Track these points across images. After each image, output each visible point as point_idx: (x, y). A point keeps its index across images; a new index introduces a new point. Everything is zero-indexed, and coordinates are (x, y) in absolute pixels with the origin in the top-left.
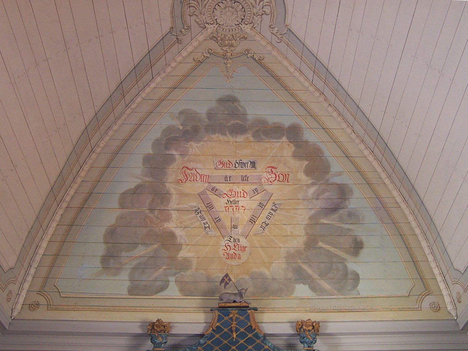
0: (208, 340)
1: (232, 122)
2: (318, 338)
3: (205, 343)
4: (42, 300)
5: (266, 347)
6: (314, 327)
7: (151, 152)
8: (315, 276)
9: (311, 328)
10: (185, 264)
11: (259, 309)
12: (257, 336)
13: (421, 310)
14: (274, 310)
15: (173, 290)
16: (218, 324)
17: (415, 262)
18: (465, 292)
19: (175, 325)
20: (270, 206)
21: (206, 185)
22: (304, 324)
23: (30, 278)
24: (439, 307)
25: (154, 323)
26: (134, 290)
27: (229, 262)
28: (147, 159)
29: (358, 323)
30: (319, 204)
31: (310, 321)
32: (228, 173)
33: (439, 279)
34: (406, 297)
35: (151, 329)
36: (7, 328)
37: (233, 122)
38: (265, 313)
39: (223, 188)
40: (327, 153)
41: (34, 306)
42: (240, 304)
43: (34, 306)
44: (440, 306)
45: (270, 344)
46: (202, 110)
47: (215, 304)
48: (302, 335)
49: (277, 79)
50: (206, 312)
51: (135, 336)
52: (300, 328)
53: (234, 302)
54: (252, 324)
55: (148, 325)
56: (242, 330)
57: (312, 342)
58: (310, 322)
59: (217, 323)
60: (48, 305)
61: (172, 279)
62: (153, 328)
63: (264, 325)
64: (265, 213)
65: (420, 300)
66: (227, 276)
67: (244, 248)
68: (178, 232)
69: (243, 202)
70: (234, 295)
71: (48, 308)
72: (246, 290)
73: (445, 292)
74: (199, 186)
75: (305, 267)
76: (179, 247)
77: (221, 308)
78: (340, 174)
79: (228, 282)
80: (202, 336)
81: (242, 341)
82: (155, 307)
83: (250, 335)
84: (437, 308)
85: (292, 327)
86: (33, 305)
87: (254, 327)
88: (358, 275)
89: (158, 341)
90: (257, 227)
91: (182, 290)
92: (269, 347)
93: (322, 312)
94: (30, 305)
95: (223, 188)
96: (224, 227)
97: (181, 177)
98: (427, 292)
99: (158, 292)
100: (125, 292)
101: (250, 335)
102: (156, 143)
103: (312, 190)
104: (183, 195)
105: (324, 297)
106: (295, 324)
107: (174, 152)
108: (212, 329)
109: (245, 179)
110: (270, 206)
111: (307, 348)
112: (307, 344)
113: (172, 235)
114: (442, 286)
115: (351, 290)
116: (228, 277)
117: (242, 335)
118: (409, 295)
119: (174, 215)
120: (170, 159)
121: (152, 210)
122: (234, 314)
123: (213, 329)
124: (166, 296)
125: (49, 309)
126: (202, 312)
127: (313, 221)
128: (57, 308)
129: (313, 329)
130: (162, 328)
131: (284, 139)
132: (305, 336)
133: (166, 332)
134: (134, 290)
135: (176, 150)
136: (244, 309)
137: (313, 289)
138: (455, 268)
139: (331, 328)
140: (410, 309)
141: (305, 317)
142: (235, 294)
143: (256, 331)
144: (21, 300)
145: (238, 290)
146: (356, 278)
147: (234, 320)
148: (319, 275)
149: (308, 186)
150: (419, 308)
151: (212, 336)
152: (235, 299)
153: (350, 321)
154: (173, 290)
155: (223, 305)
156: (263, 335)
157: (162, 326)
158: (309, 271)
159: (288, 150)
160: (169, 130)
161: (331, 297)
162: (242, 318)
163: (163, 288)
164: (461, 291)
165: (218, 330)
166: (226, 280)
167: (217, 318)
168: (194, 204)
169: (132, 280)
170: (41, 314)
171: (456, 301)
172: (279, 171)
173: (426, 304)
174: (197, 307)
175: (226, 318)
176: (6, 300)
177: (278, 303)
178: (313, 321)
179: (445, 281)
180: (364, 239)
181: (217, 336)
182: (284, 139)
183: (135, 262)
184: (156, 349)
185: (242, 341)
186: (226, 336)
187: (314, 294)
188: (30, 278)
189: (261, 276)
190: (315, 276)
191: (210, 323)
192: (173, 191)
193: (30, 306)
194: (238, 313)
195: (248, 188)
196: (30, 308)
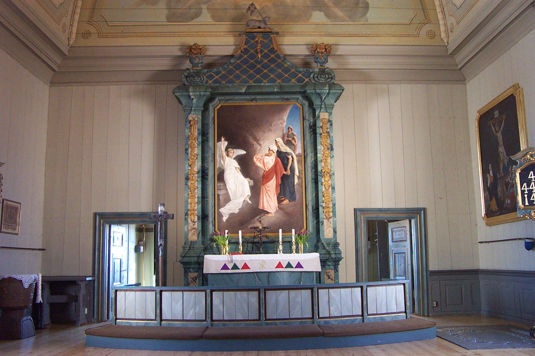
0: (237, 60)
2: (329, 58)
3: (235, 62)
4: (92, 29)
5: (286, 66)
6: (326, 49)
9: (323, 50)
11: (280, 33)
12: (278, 56)
13: (418, 37)
14: (292, 34)
15: (206, 17)
16: (245, 47)
18: (458, 25)
19: (209, 47)
22: (318, 47)
23: (78, 10)
24: (435, 35)
25: (191, 47)
26: (171, 18)
31: (323, 45)
33: (438, 10)
34: (407, 25)
35: (189, 52)
36: (67, 54)
38: (285, 36)
41: (86, 35)
42: (264, 29)
43: (86, 35)
44: (436, 34)
45: (289, 63)
48: (316, 56)
50: (235, 36)
51: (176, 57)
52: (315, 50)
53: (259, 28)
54: (274, 46)
55: (186, 48)
56: (266, 51)
57: (324, 62)
58: (323, 46)
59: (245, 45)
60: (98, 33)
61: (204, 7)
62: (191, 51)
63: (284, 47)
65: (419, 28)
66: (252, 5)
70: (259, 22)
71: (99, 36)
72: (269, 18)
73: (441, 22)
77: (248, 33)
79: (254, 10)
80: (232, 56)
81: (266, 61)
82: (191, 32)
83: (272, 56)
84: (432, 35)
85: (308, 49)
86: (85, 34)
87: (276, 49)
88: (368, 4)
89: (195, 62)
91: (213, 17)
92: (288, 65)
93: (334, 36)
94: (82, 33)
98: (427, 20)
100: (164, 19)
101: (272, 56)
105: (337, 23)
106: (311, 46)
108: (240, 51)
111: (320, 67)
112: (320, 64)
114: (440, 16)
115: (360, 17)
116: (254, 6)
117: (265, 56)
118: (410, 24)
122: (259, 38)
123: (241, 51)
124: (199, 22)
125: (100, 37)
126: (231, 36)
129: (325, 51)
130: (198, 51)
132: (318, 57)
133: (202, 54)
134: (171, 18)
136: (267, 34)
137: (328, 16)
138: (453, 3)
139: (341, 51)
140: (408, 36)
141: (320, 40)
142: (260, 21)
143: (277, 52)
144: (75, 30)
145: (263, 18)
147: (259, 43)
148: (334, 4)
150: (417, 34)
151: (241, 57)
152: (259, 26)
153: (358, 45)
154: (206, 17)
155: (250, 30)
156: (283, 56)
157: (198, 49)
161: (343, 23)
162: (266, 41)
163: (197, 15)
164: (455, 23)
165: (246, 51)
166: (252, 8)
167: (244, 41)
169: (169, 8)
170: (94, 41)
171: (449, 30)
173: (423, 31)
174: (227, 32)
175: (252, 41)
176: (62, 32)
177: (297, 28)
178: (326, 43)
179: (443, 12)
181: (245, 56)
184: (194, 68)
185: (266, 61)
186: (252, 57)
187: (329, 20)
188: (78, 10)
191: (239, 45)
193: (83, 35)
194: (262, 37)
196: (83, 36)
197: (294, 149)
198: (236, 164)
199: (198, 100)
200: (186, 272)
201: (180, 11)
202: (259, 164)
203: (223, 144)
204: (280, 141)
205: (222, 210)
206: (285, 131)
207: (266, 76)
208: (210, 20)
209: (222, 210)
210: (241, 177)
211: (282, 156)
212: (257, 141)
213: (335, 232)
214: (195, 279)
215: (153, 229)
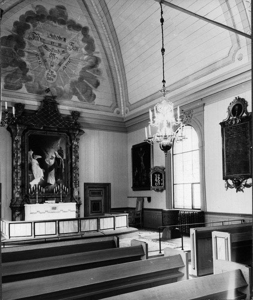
1: (60, 18)
7: (18, 20)
8: (80, 93)
10: (30, 79)
15: (24, 89)
17: (116, 95)
20: (68, 60)
21: (42, 44)
27: (49, 81)
28: (16, 23)
30: (88, 64)
32: (53, 41)
37: (60, 18)
39: (50, 47)
40: (95, 43)
46: (48, 8)
47: (42, 98)
49: (86, 6)
53: (51, 100)
61: (24, 84)
68: (28, 63)
69: (57, 55)
73: (122, 108)
74: (40, 43)
75: (77, 89)
76: (27, 70)
78: (98, 53)
80: (36, 111)
84: (118, 113)
90: (61, 68)
95: (50, 47)
96: (48, 65)
97: (31, 37)
98: (117, 106)
99: (17, 89)
102: (22, 17)
103: (86, 57)
104: (31, 45)
107: (30, 24)
109: (60, 45)
110: (68, 60)
113: (25, 63)
119: (26, 54)
120: (28, 27)
121: (16, 49)
127: (84, 70)
131: (80, 32)
135: (31, 23)
137: (79, 98)
146: (95, 97)
149: (85, 55)
154: (24, 89)
159: (81, 37)
160: (29, 12)
163: (20, 88)
168: (36, 51)
172: (74, 45)
177: (66, 102)
180: (101, 82)
182: (80, 32)
183: (7, 73)
189: (60, 89)
190: (80, 93)
192: (27, 42)
195: (61, 50)
197: (63, 157)
199: (20, 130)
201: (11, 84)
204: (57, 153)
205: (31, 183)
206: (59, 149)
207: (52, 123)
208: (26, 91)
209: (31, 183)
210: (40, 168)
211: (57, 159)
212: (47, 152)
213: (79, 193)
214: (18, 215)
215: (24, 220)
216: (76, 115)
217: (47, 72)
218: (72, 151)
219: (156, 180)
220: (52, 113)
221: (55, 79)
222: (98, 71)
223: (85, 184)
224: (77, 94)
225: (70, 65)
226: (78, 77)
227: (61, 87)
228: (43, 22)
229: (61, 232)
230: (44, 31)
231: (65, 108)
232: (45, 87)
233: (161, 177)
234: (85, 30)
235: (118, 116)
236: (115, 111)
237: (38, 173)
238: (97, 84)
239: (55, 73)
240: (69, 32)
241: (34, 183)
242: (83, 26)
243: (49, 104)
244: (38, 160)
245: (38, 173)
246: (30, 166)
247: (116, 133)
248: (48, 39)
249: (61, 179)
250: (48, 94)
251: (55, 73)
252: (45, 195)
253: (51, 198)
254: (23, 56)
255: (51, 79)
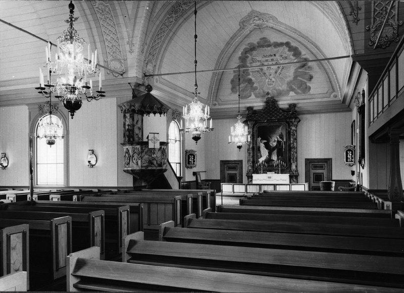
8: (296, 89)
10: (256, 89)
15: (253, 96)
17: (331, 82)
28: (240, 58)
29: (199, 229)
30: (298, 65)
32: (267, 59)
39: (266, 63)
40: (300, 49)
47: (265, 100)
61: (252, 93)
64: (280, 70)
67: (273, 82)
68: (253, 79)
74: (258, 64)
76: (253, 83)
78: (305, 55)
95: (266, 63)
98: (334, 90)
109: (272, 60)
119: (251, 73)
120: (248, 57)
128: (222, 105)
146: (310, 88)
154: (253, 96)
158: (294, 87)
159: (286, 49)
160: (245, 49)
163: (250, 96)
195: (274, 63)
197: (283, 140)
198: (263, 145)
200: (248, 179)
202: (271, 145)
203: (260, 139)
205: (259, 160)
209: (259, 160)
211: (279, 142)
216: (293, 106)
217: (267, 80)
218: (291, 135)
219: (348, 156)
220: (273, 109)
221: (274, 84)
222: (309, 67)
223: (307, 160)
224: (293, 90)
225: (284, 71)
226: (293, 77)
227: (280, 88)
228: (255, 51)
229: (248, 192)
230: (258, 55)
231: (283, 103)
232: (267, 91)
233: (352, 154)
234: (287, 44)
235: (336, 99)
236: (332, 96)
237: (265, 153)
238: (311, 78)
239: (273, 79)
240: (276, 50)
241: (261, 160)
242: (285, 42)
243: (271, 104)
244: (264, 143)
245: (265, 153)
246: (259, 147)
247: (338, 114)
248: (263, 59)
249: (282, 156)
250: (269, 96)
251: (273, 79)
252: (269, 167)
253: (270, 171)
254: (249, 75)
255: (271, 84)
